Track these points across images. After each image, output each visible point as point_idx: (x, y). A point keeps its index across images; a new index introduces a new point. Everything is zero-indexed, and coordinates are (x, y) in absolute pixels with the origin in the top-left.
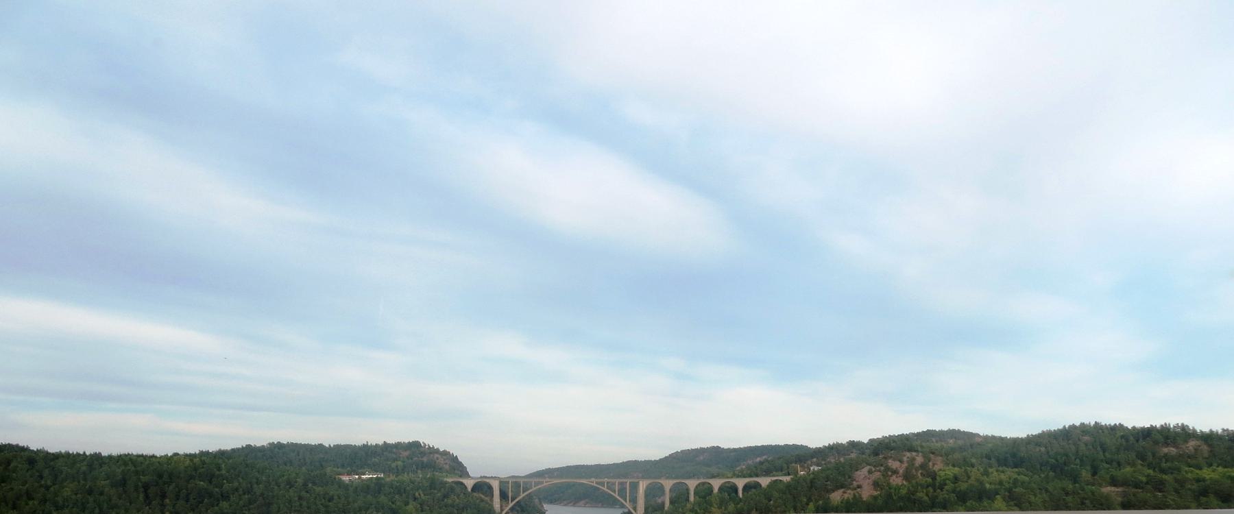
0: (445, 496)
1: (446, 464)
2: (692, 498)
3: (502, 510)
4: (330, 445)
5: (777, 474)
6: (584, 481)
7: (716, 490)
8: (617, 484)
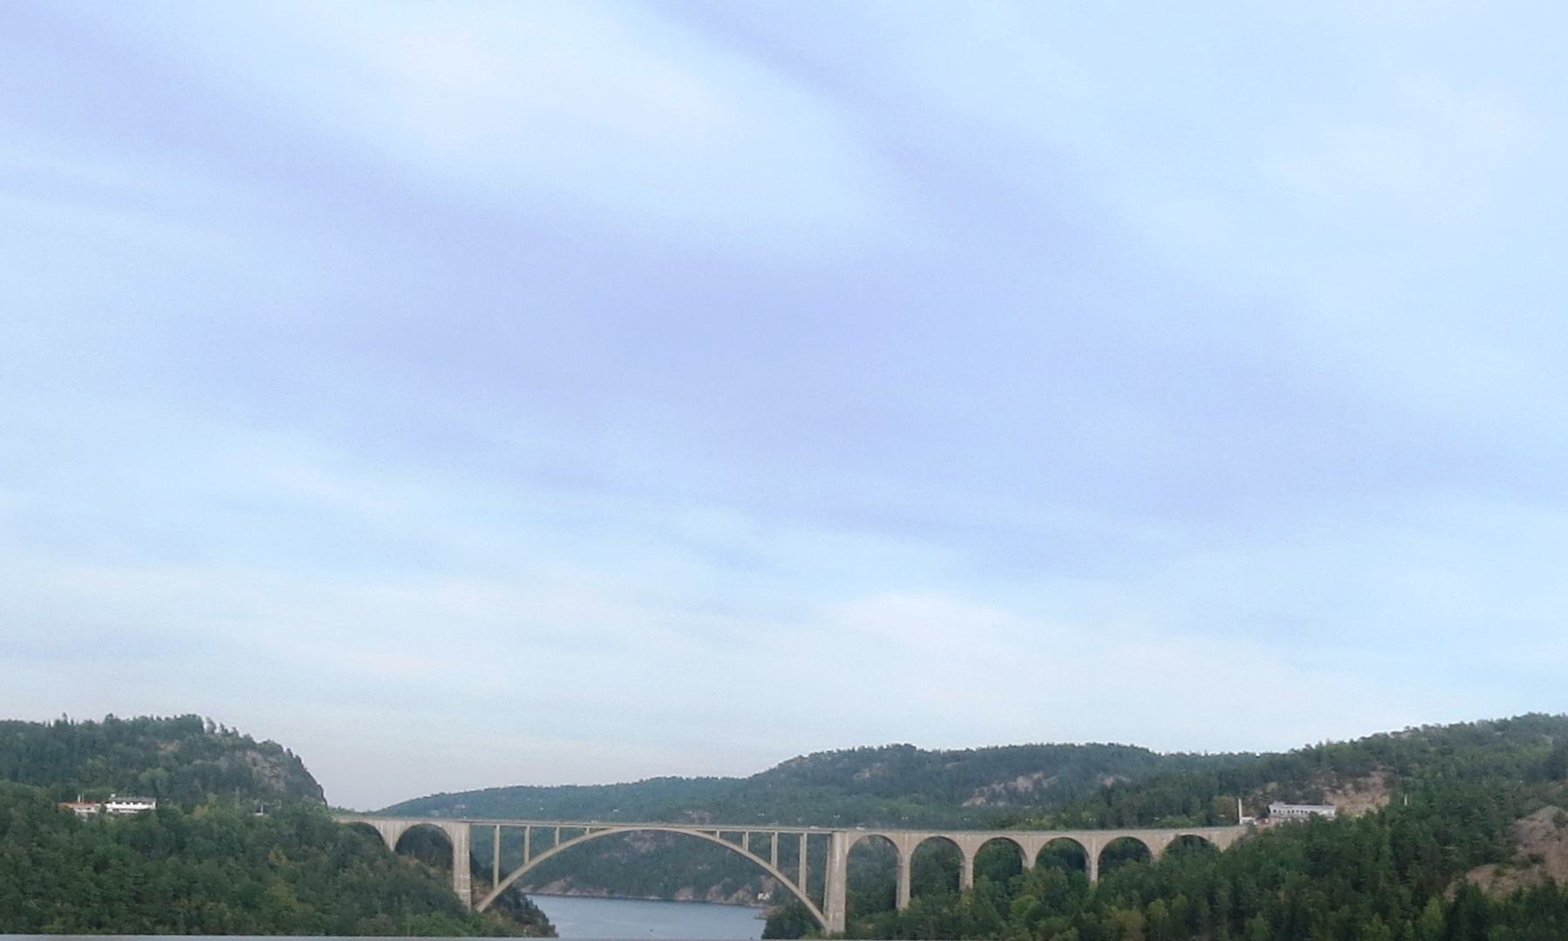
0: (342, 864)
1: (277, 776)
2: (968, 879)
3: (474, 903)
4: (175, 717)
5: (1178, 820)
7: (1030, 862)
8: (557, 833)
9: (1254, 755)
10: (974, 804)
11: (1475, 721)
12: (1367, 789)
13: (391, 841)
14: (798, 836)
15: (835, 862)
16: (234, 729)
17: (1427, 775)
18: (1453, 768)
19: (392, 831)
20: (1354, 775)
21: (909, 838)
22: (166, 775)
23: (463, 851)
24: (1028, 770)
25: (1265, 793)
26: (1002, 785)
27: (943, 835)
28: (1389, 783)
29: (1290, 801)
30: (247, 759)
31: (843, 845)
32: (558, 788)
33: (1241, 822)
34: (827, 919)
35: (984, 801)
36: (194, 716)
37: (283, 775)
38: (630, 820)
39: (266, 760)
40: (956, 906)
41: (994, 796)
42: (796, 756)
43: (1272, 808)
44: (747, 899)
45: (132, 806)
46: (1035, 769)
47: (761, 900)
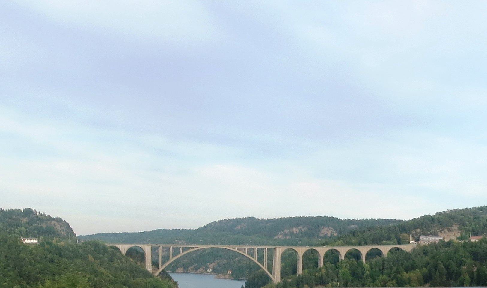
1: (63, 230)
2: (321, 264)
6: (236, 248)
7: (342, 257)
9: (375, 219)
10: (278, 238)
11: (471, 208)
12: (452, 231)
13: (124, 252)
14: (169, 248)
15: (277, 258)
16: (44, 213)
17: (473, 226)
18: (482, 223)
19: (124, 248)
20: (447, 226)
21: (302, 249)
22: (25, 230)
23: (149, 255)
24: (297, 225)
25: (416, 233)
26: (288, 231)
27: (313, 248)
28: (460, 229)
29: (427, 235)
30: (52, 224)
31: (279, 252)
32: (121, 233)
33: (410, 242)
34: (274, 278)
35: (282, 236)
36: (30, 209)
37: (65, 229)
38: (205, 243)
39: (59, 224)
40: (320, 272)
41: (285, 235)
42: (214, 221)
43: (421, 238)
44: (203, 272)
45: (29, 241)
46: (299, 225)
47: (209, 272)
